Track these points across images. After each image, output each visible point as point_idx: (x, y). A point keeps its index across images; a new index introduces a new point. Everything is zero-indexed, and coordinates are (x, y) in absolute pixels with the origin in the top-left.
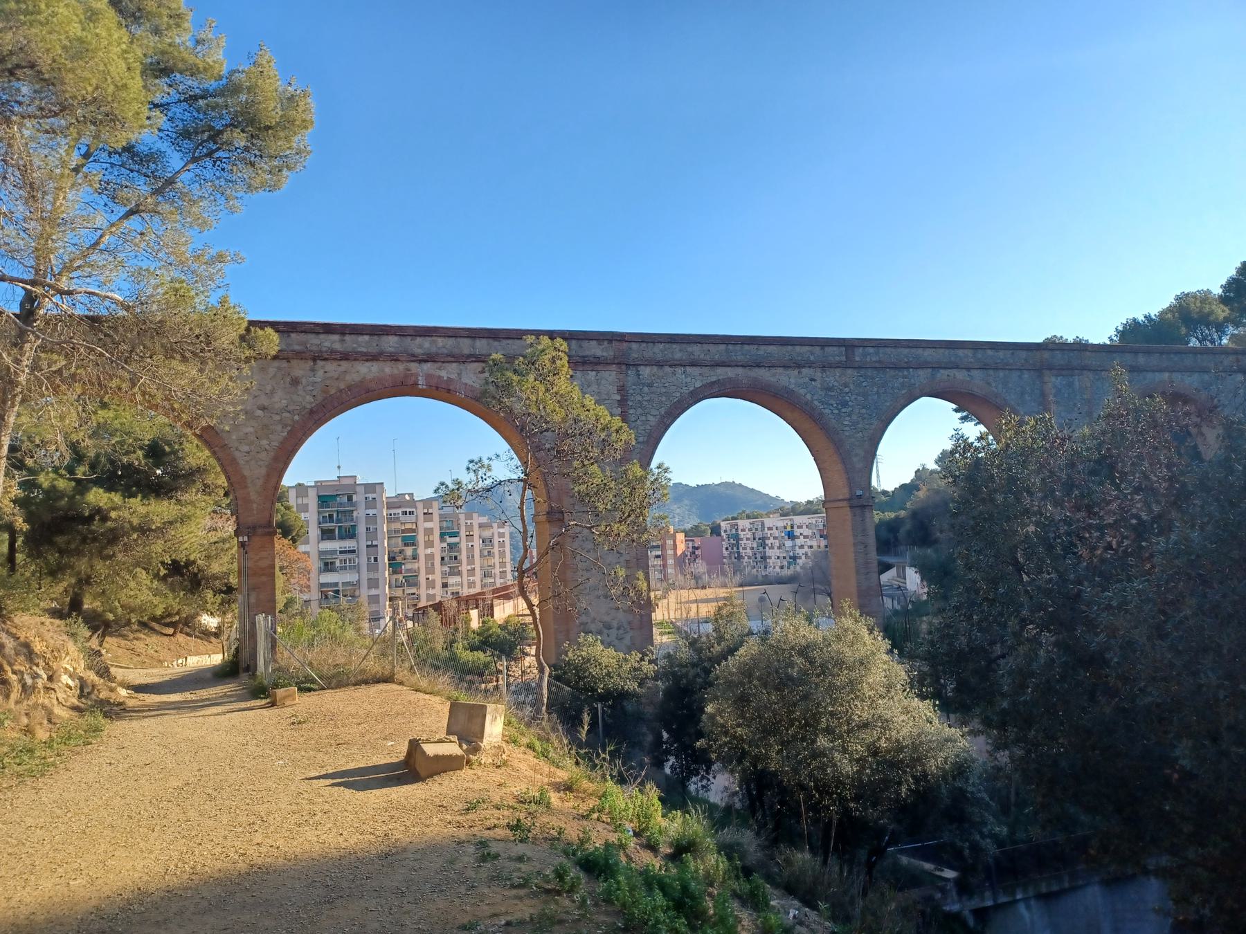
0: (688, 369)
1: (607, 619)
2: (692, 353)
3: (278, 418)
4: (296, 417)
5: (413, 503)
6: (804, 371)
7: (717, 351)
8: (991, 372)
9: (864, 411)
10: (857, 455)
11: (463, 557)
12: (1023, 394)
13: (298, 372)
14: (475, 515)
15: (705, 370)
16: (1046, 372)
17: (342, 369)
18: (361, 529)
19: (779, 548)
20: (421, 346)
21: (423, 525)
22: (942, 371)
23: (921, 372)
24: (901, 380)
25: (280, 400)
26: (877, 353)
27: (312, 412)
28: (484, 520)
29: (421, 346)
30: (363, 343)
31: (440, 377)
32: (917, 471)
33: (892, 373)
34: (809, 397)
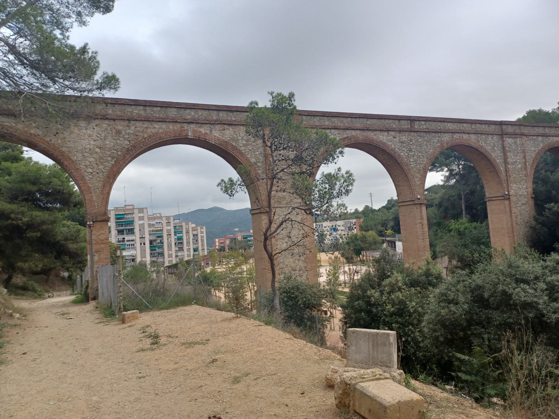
0: (333, 131)
1: (293, 265)
2: (334, 122)
3: (109, 153)
4: (119, 153)
5: (161, 217)
6: (391, 133)
7: (347, 122)
8: (479, 135)
9: (420, 154)
10: (417, 177)
11: (185, 241)
12: (494, 147)
13: (120, 128)
14: (190, 223)
15: (341, 131)
16: (504, 136)
17: (146, 126)
18: (137, 230)
19: (330, 235)
20: (190, 114)
21: (166, 228)
22: (457, 134)
23: (447, 135)
24: (437, 138)
25: (109, 143)
26: (426, 124)
27: (128, 150)
28: (194, 225)
29: (190, 114)
30: (157, 112)
31: (200, 132)
32: (389, 201)
33: (433, 134)
34: (393, 146)
